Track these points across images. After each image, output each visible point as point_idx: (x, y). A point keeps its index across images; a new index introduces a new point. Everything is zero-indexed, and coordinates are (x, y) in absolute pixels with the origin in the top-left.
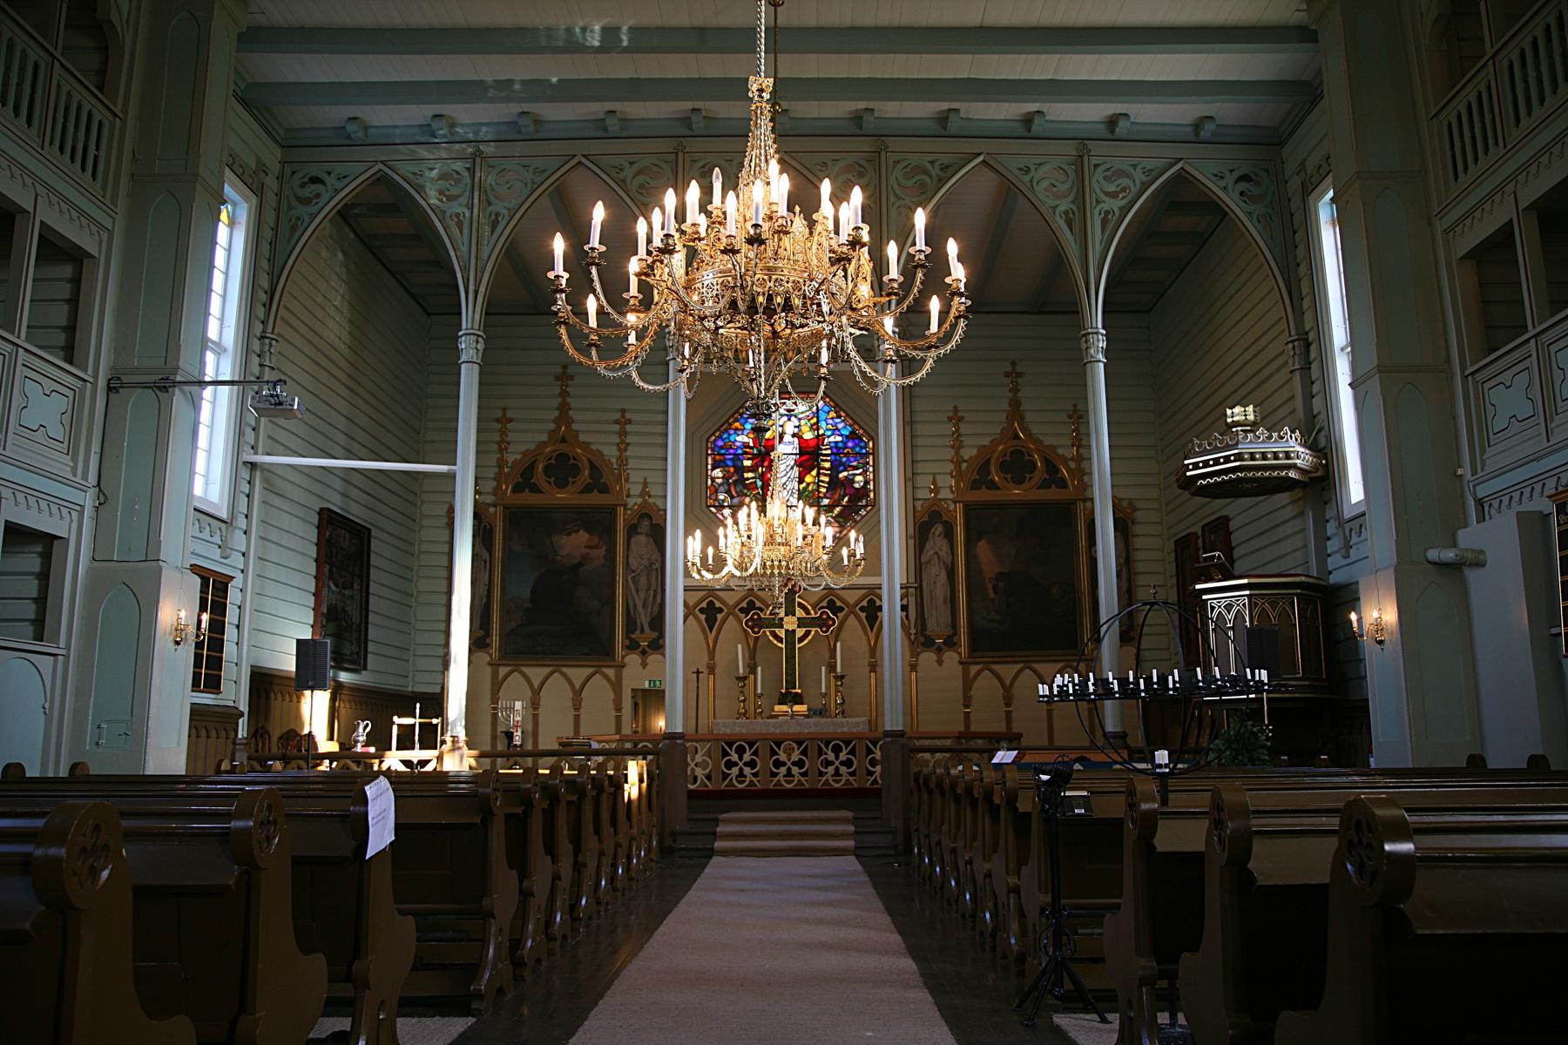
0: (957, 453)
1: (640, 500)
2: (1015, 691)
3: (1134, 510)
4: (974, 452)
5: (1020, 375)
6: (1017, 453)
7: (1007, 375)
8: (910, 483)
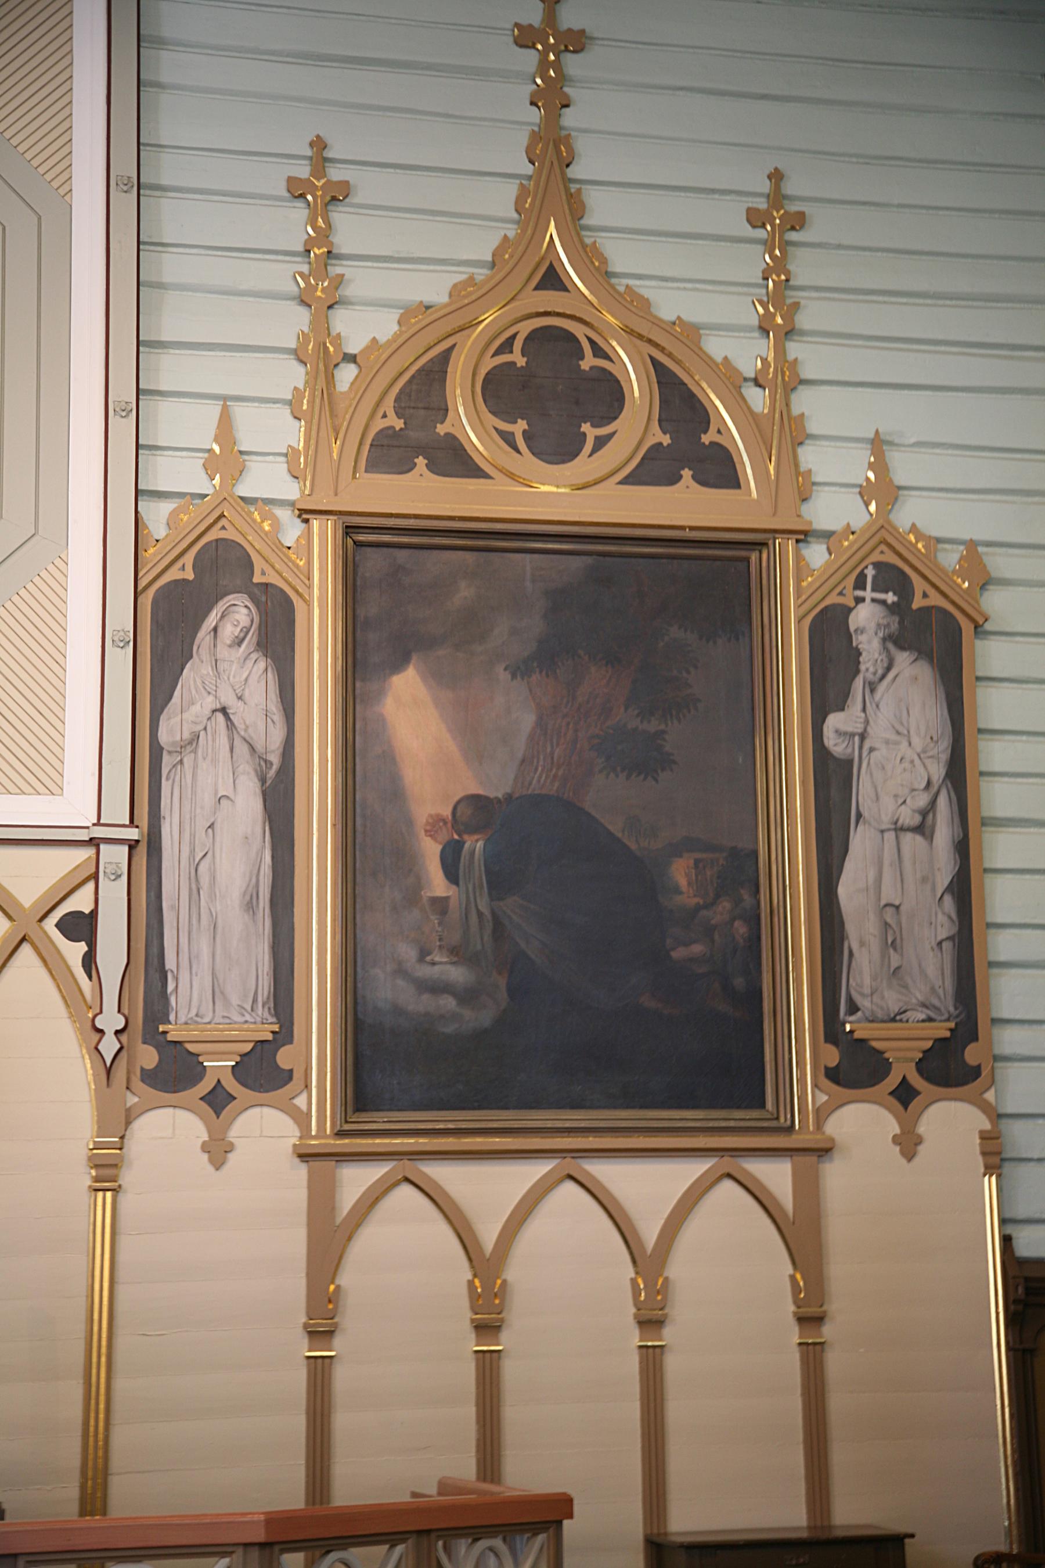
0: (321, 326)
2: (514, 1273)
3: (986, 582)
4: (385, 326)
5: (576, 42)
6: (554, 343)
7: (525, 38)
8: (123, 429)
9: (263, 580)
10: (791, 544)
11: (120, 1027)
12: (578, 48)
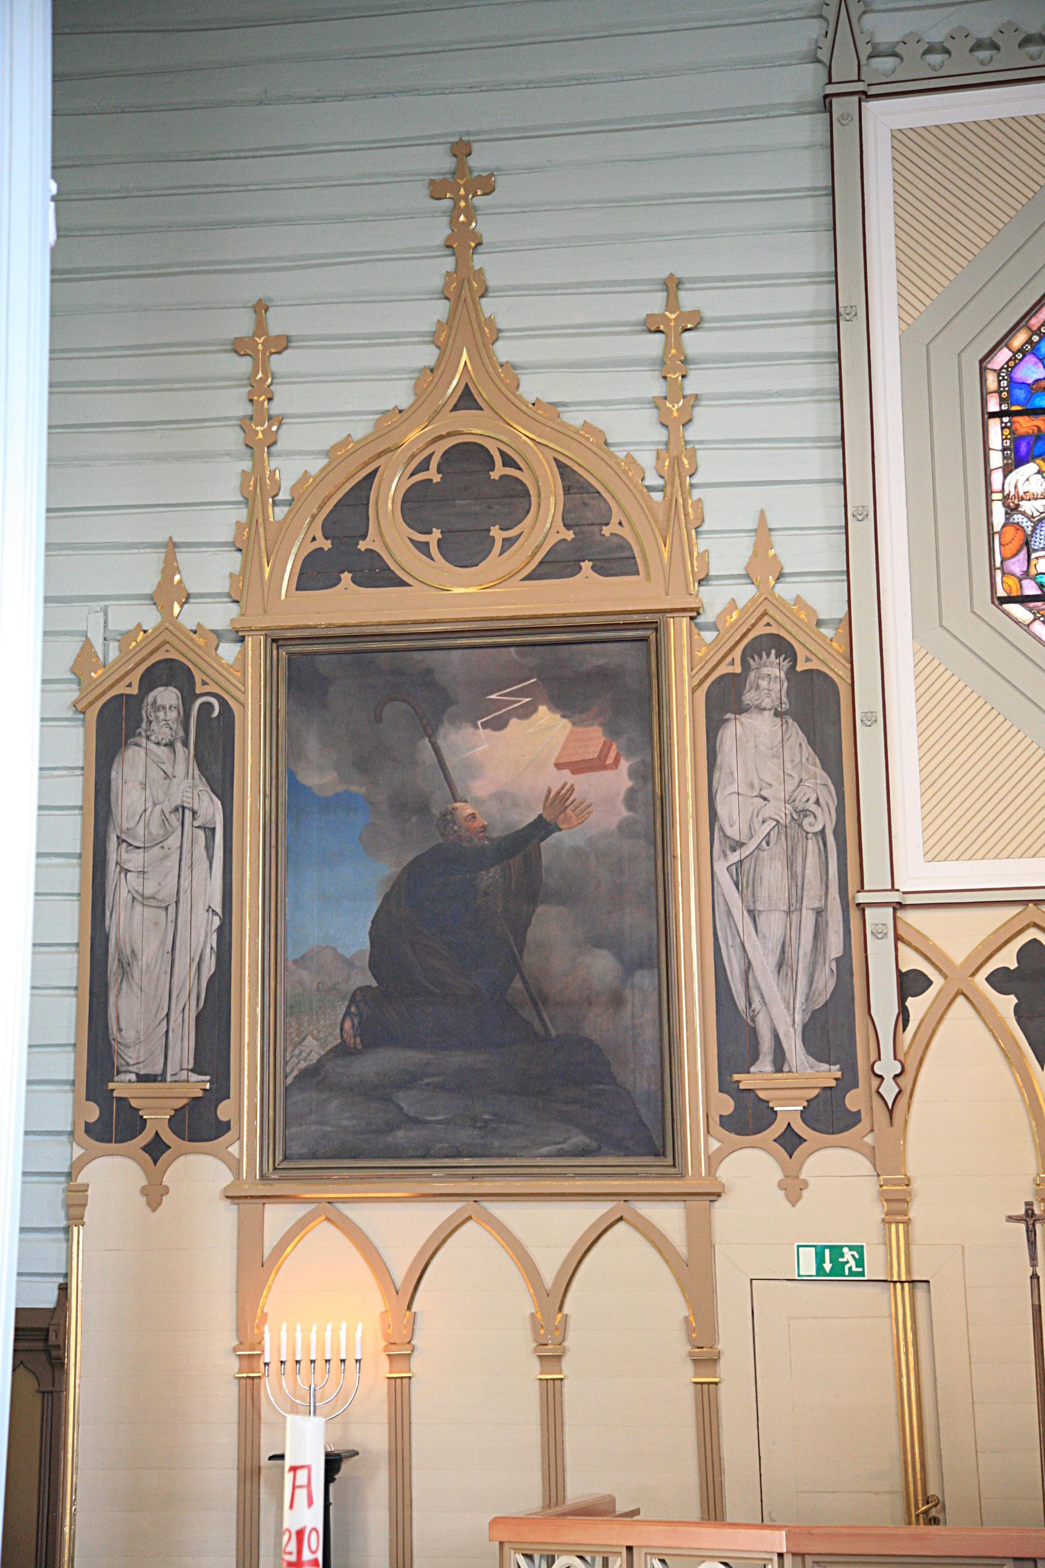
1: (745, 593)
9: (808, 666)
10: (685, 621)
11: (898, 1071)
12: (488, 191)
